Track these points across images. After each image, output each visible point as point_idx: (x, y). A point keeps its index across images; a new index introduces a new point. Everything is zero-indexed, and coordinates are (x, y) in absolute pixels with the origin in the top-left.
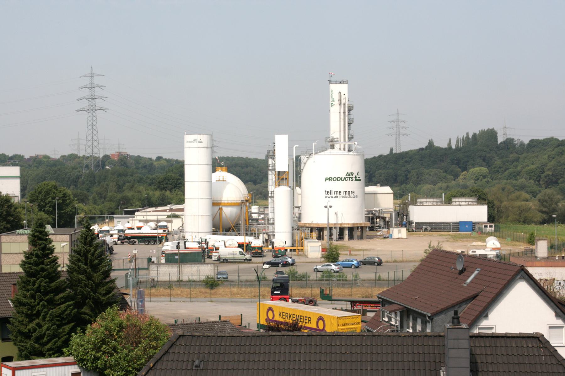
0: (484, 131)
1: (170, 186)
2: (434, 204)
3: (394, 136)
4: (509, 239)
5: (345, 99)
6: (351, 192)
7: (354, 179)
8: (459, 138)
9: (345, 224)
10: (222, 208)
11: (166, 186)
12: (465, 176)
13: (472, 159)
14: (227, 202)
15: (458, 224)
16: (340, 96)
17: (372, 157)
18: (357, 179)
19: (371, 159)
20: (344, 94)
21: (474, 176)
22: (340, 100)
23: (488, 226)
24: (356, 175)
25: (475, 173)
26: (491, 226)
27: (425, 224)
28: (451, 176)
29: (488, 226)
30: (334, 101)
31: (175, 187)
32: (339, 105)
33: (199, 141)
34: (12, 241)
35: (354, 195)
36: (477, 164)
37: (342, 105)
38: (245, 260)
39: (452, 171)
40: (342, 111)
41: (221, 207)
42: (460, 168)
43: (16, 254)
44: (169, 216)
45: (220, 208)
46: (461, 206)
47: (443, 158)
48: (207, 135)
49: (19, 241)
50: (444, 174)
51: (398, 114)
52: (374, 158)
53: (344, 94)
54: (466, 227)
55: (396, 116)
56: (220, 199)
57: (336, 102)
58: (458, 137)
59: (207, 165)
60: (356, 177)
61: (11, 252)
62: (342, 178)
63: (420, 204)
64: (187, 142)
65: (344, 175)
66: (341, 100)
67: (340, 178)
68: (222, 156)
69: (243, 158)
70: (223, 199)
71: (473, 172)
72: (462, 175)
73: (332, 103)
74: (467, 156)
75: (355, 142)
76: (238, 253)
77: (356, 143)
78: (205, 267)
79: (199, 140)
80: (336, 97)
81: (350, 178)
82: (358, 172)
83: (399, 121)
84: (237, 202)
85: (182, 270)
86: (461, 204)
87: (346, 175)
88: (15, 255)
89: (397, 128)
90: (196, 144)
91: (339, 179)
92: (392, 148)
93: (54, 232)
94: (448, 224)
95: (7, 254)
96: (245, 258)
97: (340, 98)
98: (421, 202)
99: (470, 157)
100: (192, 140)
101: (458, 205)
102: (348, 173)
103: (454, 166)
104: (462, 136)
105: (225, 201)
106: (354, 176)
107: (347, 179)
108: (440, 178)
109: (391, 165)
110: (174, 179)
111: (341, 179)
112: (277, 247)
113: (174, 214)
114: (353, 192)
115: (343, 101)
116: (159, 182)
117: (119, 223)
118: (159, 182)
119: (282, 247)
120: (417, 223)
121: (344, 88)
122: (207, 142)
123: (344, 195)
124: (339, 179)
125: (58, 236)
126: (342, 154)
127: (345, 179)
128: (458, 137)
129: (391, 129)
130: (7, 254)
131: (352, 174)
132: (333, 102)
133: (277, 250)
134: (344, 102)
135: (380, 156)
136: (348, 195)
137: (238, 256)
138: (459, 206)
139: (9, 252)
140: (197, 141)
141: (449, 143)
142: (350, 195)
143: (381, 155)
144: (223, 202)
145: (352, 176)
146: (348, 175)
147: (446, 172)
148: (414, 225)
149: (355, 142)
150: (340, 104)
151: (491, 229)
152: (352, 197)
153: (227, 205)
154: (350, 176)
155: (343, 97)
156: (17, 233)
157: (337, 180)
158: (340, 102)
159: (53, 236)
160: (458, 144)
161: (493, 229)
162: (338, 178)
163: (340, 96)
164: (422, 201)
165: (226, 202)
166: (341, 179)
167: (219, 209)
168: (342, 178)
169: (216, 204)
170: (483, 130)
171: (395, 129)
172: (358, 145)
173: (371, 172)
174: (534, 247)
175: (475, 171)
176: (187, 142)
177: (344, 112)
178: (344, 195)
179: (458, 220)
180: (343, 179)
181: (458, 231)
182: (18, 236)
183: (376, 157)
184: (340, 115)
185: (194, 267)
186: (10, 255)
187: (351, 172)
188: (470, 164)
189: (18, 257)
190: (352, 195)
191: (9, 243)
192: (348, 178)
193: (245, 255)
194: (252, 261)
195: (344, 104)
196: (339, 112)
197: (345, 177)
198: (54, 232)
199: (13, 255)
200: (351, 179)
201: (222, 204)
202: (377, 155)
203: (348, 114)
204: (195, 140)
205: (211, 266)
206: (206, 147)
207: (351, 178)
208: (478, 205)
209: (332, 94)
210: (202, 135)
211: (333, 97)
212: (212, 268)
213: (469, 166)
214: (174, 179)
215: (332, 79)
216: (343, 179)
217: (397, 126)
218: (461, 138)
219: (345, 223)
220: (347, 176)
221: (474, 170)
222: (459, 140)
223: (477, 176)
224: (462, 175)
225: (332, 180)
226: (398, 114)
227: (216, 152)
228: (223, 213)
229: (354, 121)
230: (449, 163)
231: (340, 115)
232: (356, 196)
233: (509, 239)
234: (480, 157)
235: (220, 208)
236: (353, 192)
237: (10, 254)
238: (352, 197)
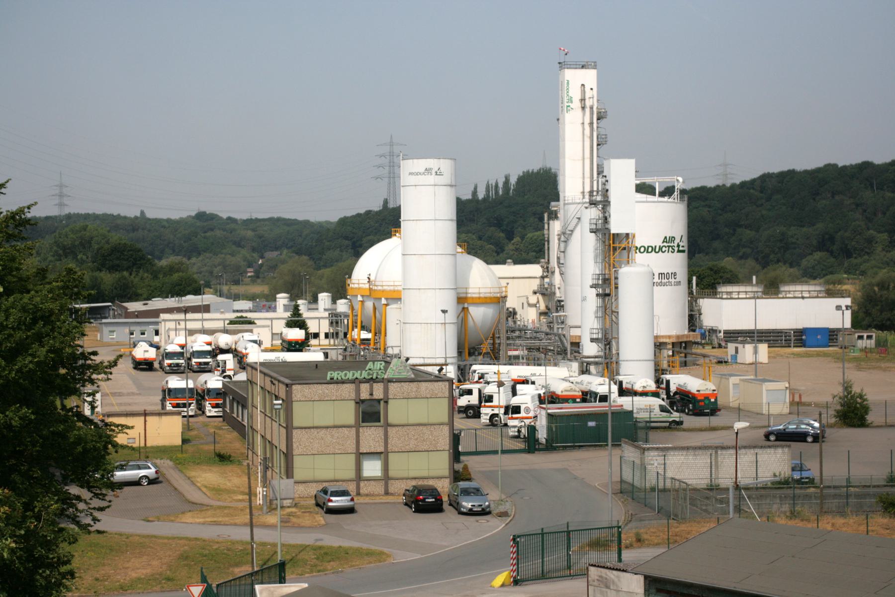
0: (533, 172)
1: (125, 262)
2: (796, 295)
3: (386, 180)
4: (300, 342)
5: (593, 98)
6: (672, 274)
7: (676, 249)
8: (490, 183)
9: (663, 337)
10: (467, 308)
11: (118, 262)
12: (517, 245)
13: (521, 217)
14: (477, 295)
15: (802, 332)
16: (583, 92)
17: (354, 214)
18: (681, 248)
19: (353, 217)
20: (592, 89)
21: (534, 245)
22: (583, 100)
23: (865, 337)
24: (679, 241)
25: (536, 240)
26: (869, 337)
27: (741, 333)
28: (491, 246)
29: (865, 337)
30: (572, 102)
31: (134, 264)
32: (581, 109)
33: (436, 172)
34: (317, 398)
35: (676, 280)
36: (531, 226)
37: (588, 110)
38: (671, 423)
39: (490, 238)
40: (587, 121)
41: (466, 305)
42: (503, 231)
43: (327, 427)
44: (232, 322)
45: (464, 308)
46: (806, 300)
47: (474, 216)
48: (451, 159)
49: (334, 398)
50: (479, 243)
51: (391, 144)
52: (359, 215)
53: (592, 89)
54: (818, 340)
55: (389, 147)
56: (464, 291)
57: (576, 104)
58: (488, 182)
59: (450, 220)
60: (678, 246)
61: (316, 424)
62: (656, 247)
63: (744, 296)
64: (411, 174)
65: (658, 243)
66: (584, 100)
67: (652, 247)
68: (76, 212)
69: (113, 215)
70: (470, 291)
71: (531, 238)
72: (513, 244)
73: (568, 104)
74: (514, 213)
75: (679, 178)
76: (657, 409)
77: (680, 179)
78: (770, 453)
79: (436, 169)
80: (576, 94)
81: (669, 247)
82: (682, 236)
83: (393, 156)
84: (495, 295)
85: (716, 462)
86: (788, 296)
87: (663, 242)
88: (324, 431)
89: (390, 166)
90: (431, 179)
91: (650, 249)
92: (387, 199)
93: (413, 376)
94: (781, 333)
95: (305, 428)
96: (671, 420)
97: (584, 97)
98: (727, 293)
99: (518, 214)
100: (422, 170)
101: (799, 298)
102: (666, 238)
103: (492, 228)
104: (495, 181)
105: (474, 293)
106: (676, 245)
107: (664, 249)
108: (473, 249)
109: (388, 228)
110: (131, 250)
111: (654, 249)
112: (701, 392)
113: (242, 317)
114: (675, 274)
115: (588, 103)
116: (103, 256)
117: (112, 334)
118: (103, 256)
119: (711, 392)
120: (726, 332)
121: (589, 77)
122: (451, 174)
123: (659, 281)
124: (650, 249)
125: (424, 384)
126: (645, 200)
127: (661, 248)
128: (488, 182)
129: (381, 168)
130: (305, 428)
131: (672, 239)
132: (570, 104)
133: (703, 398)
134: (591, 104)
135: (368, 212)
136: (666, 280)
137: (657, 414)
138: (801, 300)
139: (311, 425)
140: (434, 173)
141: (475, 193)
142: (670, 280)
143: (370, 211)
144: (469, 295)
145: (672, 244)
146: (666, 242)
147: (480, 238)
148: (722, 334)
149: (679, 178)
150: (583, 108)
151: (869, 341)
152: (673, 284)
153: (478, 301)
154: (670, 244)
155: (588, 94)
156: (328, 378)
157: (648, 252)
158: (584, 104)
159: (411, 384)
160: (489, 192)
161: (873, 341)
162: (648, 247)
163: (583, 92)
164: (731, 290)
165: (474, 296)
166: (654, 249)
167: (462, 311)
168: (656, 247)
169: (462, 301)
170: (530, 171)
171: (387, 168)
172: (684, 182)
173: (355, 240)
174: (678, 368)
175: (535, 237)
176: (411, 174)
177: (591, 124)
178: (660, 281)
179: (800, 326)
180: (657, 250)
181: (801, 346)
182: (331, 386)
183: (361, 214)
184: (584, 129)
185: (746, 454)
186: (312, 430)
187: (671, 236)
188: (519, 226)
189: (332, 436)
190: (673, 280)
191: (311, 403)
192: (666, 247)
193: (671, 413)
194: (685, 426)
195: (591, 108)
196: (581, 122)
197: (662, 245)
198: (413, 376)
199: (319, 430)
200: (670, 248)
201: (470, 301)
202: (362, 211)
203: (598, 127)
204: (428, 171)
205: (783, 453)
206: (450, 184)
207: (672, 247)
208: (825, 297)
209: (568, 89)
210: (442, 160)
211: (570, 94)
212: (786, 457)
213: (517, 228)
214: (131, 250)
215: (568, 58)
216: (657, 250)
217: (390, 162)
218: (494, 184)
219: (662, 334)
220: (665, 244)
221: (533, 236)
222: (490, 186)
223: (538, 246)
224: (513, 244)
225: (638, 251)
226: (391, 144)
227: (66, 205)
228: (470, 319)
229: (608, 139)
230: (484, 223)
231: (584, 129)
232: (679, 283)
233: (300, 342)
234: (534, 214)
235: (464, 308)
236: (675, 274)
237: (313, 428)
238: (673, 284)
